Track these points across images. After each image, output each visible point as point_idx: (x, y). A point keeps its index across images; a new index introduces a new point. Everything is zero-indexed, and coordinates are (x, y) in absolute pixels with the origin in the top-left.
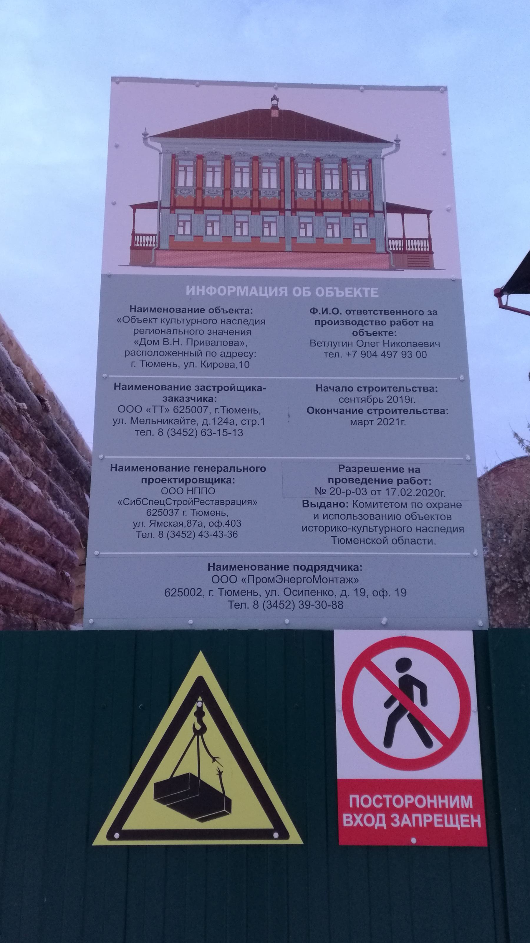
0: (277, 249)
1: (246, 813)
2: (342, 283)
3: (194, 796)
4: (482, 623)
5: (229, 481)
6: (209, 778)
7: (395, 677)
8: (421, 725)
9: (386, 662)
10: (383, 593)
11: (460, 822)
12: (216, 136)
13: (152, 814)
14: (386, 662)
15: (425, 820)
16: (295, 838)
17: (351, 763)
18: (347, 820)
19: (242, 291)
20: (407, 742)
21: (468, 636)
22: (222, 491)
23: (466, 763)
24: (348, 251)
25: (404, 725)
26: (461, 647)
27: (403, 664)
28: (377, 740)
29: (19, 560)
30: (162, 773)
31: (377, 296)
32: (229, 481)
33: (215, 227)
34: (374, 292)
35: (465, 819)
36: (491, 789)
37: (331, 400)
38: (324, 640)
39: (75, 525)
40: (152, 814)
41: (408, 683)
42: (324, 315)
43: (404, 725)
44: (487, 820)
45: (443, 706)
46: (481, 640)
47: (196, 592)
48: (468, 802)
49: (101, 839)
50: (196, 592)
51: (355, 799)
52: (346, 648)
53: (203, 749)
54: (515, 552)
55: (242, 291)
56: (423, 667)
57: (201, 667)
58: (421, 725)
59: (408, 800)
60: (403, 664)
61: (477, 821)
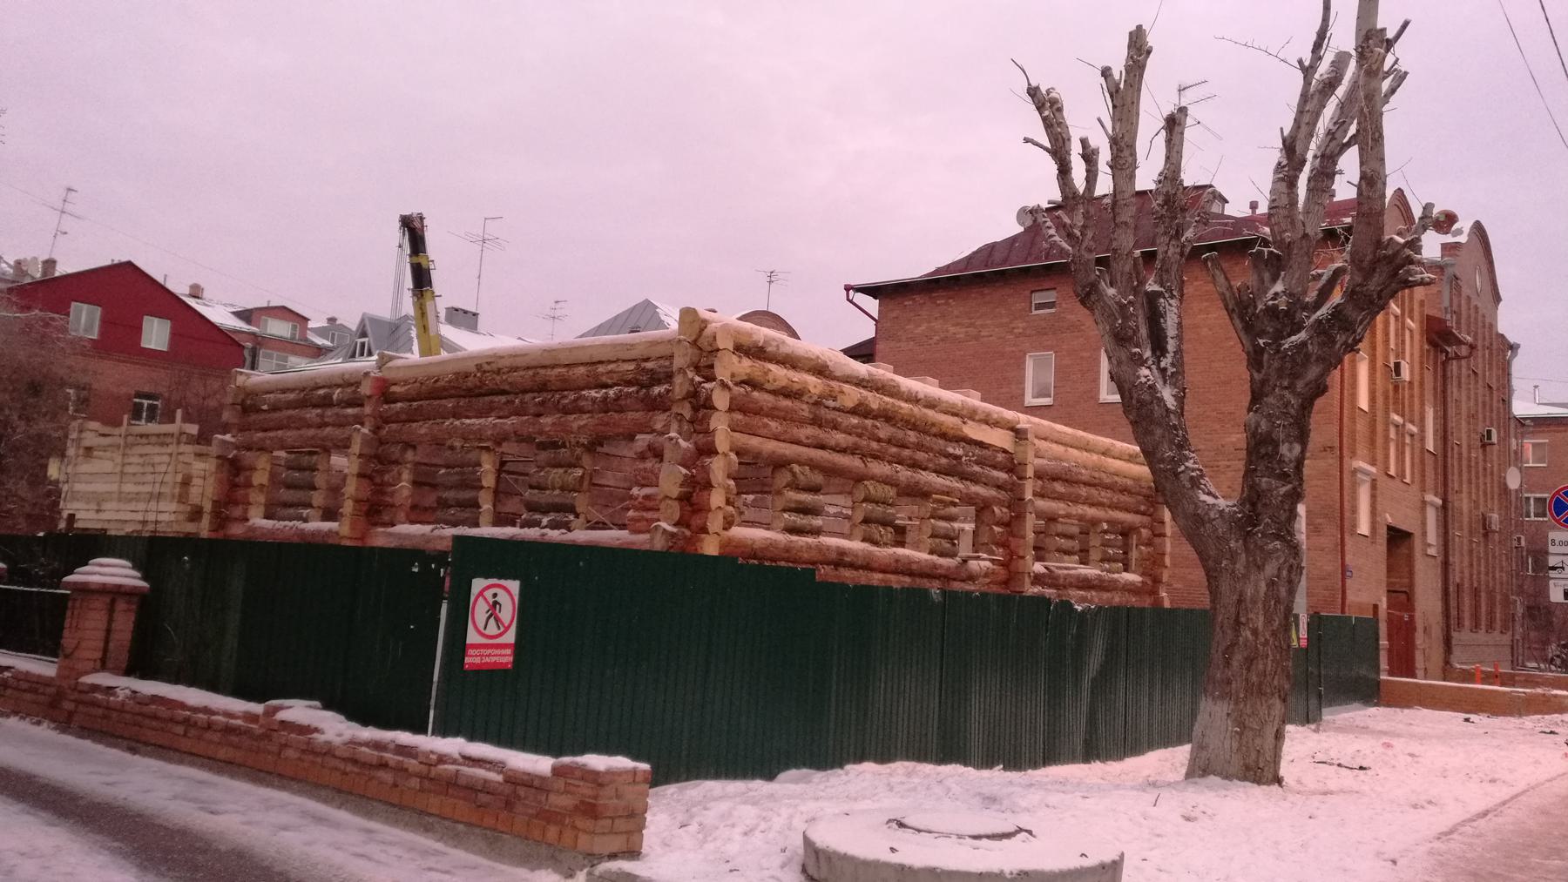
5: (1174, 124)
7: (491, 600)
8: (497, 620)
9: (489, 594)
12: (83, 728)
17: (472, 637)
18: (467, 660)
20: (492, 629)
23: (510, 637)
25: (492, 620)
27: (495, 595)
31: (62, 525)
32: (1174, 124)
35: (506, 658)
36: (518, 647)
39: (895, 372)
41: (496, 603)
43: (492, 620)
48: (509, 651)
51: (471, 652)
54: (76, 411)
56: (503, 598)
58: (497, 620)
59: (489, 651)
60: (495, 595)
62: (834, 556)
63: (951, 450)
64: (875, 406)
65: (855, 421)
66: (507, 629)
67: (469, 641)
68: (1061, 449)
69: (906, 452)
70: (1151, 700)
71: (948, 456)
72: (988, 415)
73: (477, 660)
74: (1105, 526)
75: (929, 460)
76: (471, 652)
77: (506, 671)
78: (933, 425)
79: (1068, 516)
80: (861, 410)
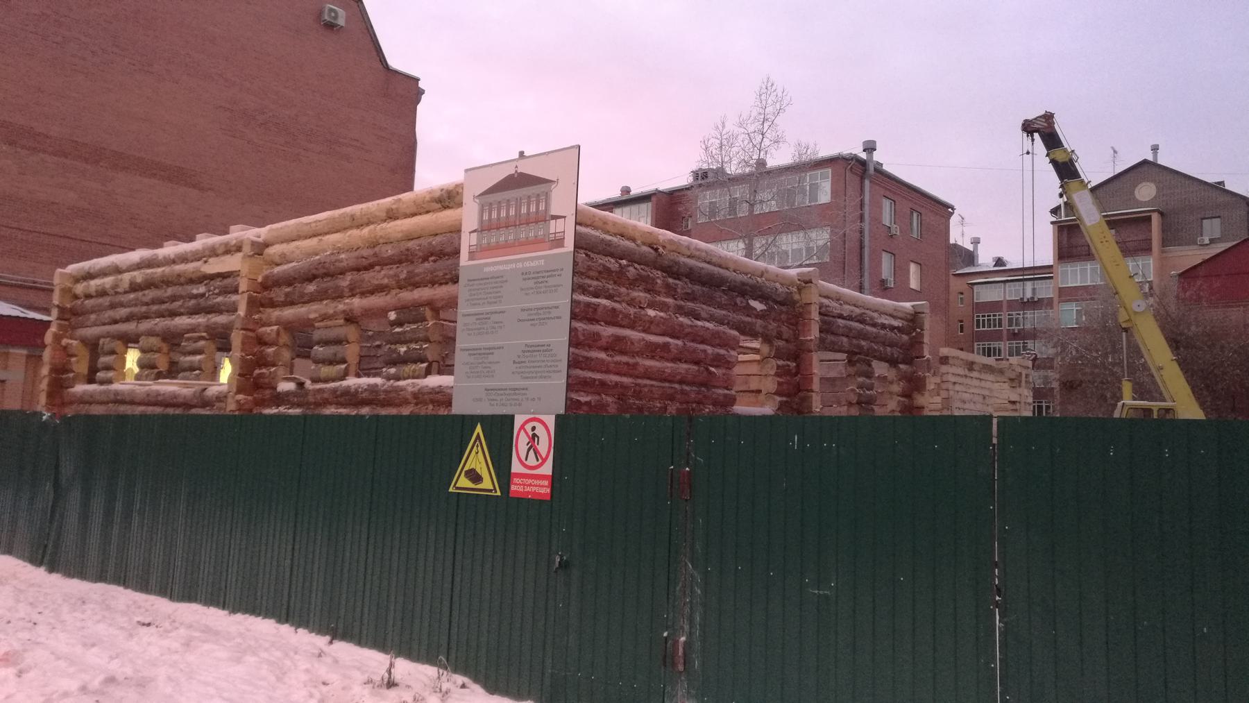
0: (512, 246)
1: (487, 484)
2: (516, 261)
3: (474, 476)
4: (562, 412)
6: (478, 471)
7: (531, 433)
10: (533, 399)
11: (543, 491)
13: (464, 482)
14: (528, 427)
15: (534, 489)
16: (499, 493)
17: (516, 467)
18: (513, 488)
19: (501, 268)
20: (532, 461)
21: (553, 417)
22: (491, 358)
23: (547, 469)
24: (537, 243)
26: (550, 421)
27: (534, 428)
28: (523, 458)
29: (635, 365)
30: (466, 468)
33: (502, 237)
34: (542, 262)
35: (544, 489)
36: (555, 479)
37: (524, 316)
38: (511, 419)
40: (464, 482)
41: (534, 435)
42: (526, 274)
44: (552, 491)
45: (544, 446)
46: (558, 417)
47: (480, 400)
48: (546, 483)
49: (451, 490)
50: (480, 400)
51: (516, 480)
52: (519, 420)
53: (477, 459)
55: (501, 268)
56: (540, 431)
57: (479, 429)
58: (536, 452)
59: (530, 481)
60: (534, 428)
61: (548, 490)
62: (112, 397)
63: (195, 292)
64: (139, 280)
65: (132, 296)
66: (544, 460)
67: (513, 470)
68: (313, 242)
69: (164, 307)
70: (85, 517)
71: (196, 297)
72: (226, 244)
73: (521, 489)
74: (392, 316)
75: (181, 306)
76: (516, 480)
77: (541, 502)
78: (179, 275)
79: (325, 317)
80: (134, 287)
